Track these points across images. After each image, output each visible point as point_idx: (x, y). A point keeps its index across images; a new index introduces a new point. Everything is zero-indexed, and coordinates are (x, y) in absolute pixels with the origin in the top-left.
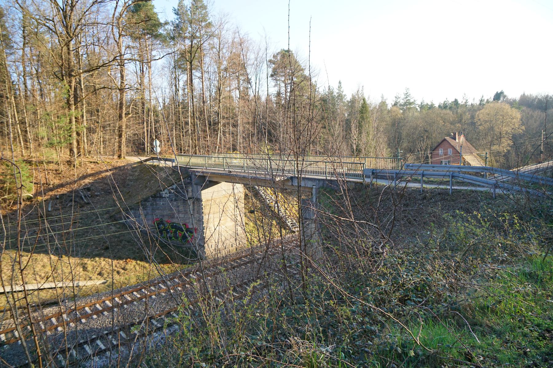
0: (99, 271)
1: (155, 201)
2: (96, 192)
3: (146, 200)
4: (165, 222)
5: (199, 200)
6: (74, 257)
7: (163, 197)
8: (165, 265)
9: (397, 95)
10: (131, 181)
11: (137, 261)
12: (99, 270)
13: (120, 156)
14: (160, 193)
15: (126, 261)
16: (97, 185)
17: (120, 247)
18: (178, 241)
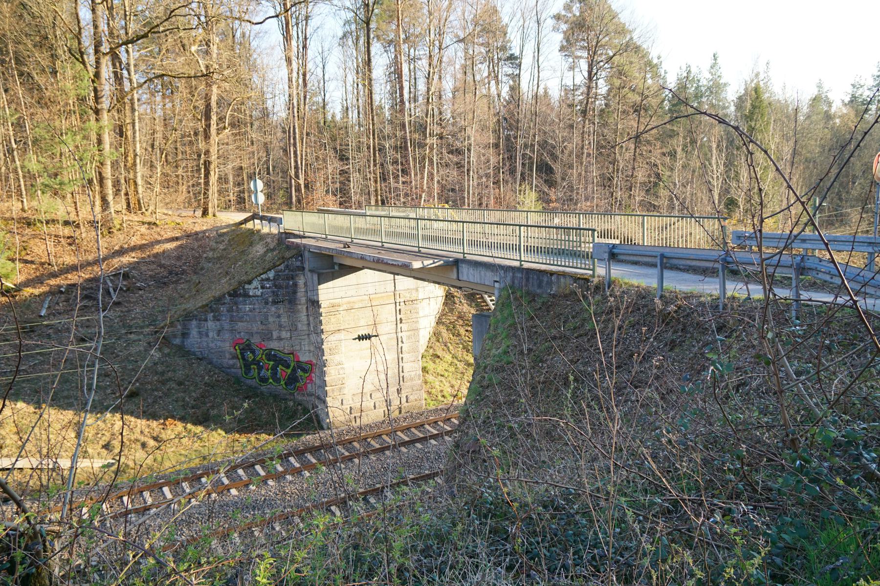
0: (107, 440)
1: (236, 304)
2: (139, 281)
3: (219, 300)
4: (254, 347)
5: (315, 304)
6: (65, 410)
7: (250, 296)
8: (243, 436)
9: (858, 79)
10: (208, 260)
11: (187, 423)
12: (106, 439)
13: (205, 213)
14: (244, 287)
15: (164, 424)
16: (144, 268)
17: (160, 394)
18: (280, 387)
